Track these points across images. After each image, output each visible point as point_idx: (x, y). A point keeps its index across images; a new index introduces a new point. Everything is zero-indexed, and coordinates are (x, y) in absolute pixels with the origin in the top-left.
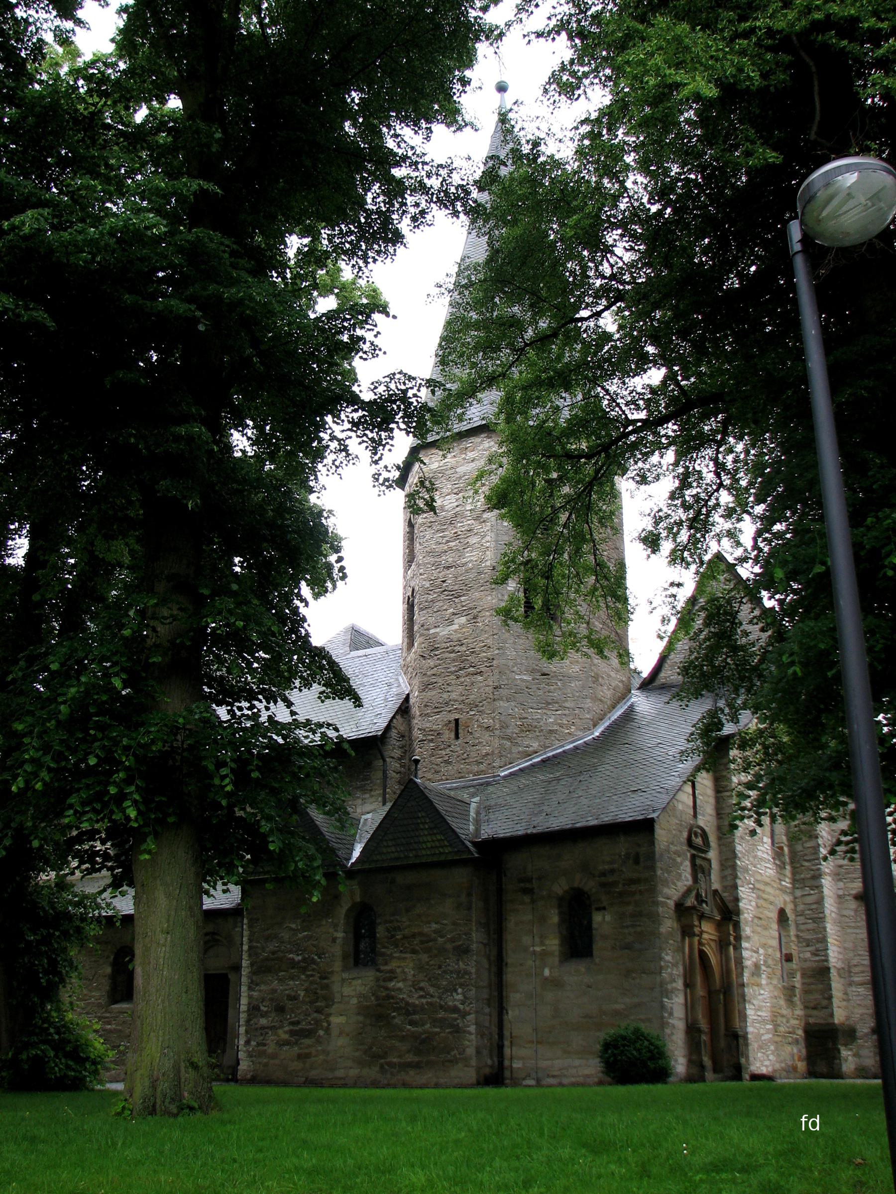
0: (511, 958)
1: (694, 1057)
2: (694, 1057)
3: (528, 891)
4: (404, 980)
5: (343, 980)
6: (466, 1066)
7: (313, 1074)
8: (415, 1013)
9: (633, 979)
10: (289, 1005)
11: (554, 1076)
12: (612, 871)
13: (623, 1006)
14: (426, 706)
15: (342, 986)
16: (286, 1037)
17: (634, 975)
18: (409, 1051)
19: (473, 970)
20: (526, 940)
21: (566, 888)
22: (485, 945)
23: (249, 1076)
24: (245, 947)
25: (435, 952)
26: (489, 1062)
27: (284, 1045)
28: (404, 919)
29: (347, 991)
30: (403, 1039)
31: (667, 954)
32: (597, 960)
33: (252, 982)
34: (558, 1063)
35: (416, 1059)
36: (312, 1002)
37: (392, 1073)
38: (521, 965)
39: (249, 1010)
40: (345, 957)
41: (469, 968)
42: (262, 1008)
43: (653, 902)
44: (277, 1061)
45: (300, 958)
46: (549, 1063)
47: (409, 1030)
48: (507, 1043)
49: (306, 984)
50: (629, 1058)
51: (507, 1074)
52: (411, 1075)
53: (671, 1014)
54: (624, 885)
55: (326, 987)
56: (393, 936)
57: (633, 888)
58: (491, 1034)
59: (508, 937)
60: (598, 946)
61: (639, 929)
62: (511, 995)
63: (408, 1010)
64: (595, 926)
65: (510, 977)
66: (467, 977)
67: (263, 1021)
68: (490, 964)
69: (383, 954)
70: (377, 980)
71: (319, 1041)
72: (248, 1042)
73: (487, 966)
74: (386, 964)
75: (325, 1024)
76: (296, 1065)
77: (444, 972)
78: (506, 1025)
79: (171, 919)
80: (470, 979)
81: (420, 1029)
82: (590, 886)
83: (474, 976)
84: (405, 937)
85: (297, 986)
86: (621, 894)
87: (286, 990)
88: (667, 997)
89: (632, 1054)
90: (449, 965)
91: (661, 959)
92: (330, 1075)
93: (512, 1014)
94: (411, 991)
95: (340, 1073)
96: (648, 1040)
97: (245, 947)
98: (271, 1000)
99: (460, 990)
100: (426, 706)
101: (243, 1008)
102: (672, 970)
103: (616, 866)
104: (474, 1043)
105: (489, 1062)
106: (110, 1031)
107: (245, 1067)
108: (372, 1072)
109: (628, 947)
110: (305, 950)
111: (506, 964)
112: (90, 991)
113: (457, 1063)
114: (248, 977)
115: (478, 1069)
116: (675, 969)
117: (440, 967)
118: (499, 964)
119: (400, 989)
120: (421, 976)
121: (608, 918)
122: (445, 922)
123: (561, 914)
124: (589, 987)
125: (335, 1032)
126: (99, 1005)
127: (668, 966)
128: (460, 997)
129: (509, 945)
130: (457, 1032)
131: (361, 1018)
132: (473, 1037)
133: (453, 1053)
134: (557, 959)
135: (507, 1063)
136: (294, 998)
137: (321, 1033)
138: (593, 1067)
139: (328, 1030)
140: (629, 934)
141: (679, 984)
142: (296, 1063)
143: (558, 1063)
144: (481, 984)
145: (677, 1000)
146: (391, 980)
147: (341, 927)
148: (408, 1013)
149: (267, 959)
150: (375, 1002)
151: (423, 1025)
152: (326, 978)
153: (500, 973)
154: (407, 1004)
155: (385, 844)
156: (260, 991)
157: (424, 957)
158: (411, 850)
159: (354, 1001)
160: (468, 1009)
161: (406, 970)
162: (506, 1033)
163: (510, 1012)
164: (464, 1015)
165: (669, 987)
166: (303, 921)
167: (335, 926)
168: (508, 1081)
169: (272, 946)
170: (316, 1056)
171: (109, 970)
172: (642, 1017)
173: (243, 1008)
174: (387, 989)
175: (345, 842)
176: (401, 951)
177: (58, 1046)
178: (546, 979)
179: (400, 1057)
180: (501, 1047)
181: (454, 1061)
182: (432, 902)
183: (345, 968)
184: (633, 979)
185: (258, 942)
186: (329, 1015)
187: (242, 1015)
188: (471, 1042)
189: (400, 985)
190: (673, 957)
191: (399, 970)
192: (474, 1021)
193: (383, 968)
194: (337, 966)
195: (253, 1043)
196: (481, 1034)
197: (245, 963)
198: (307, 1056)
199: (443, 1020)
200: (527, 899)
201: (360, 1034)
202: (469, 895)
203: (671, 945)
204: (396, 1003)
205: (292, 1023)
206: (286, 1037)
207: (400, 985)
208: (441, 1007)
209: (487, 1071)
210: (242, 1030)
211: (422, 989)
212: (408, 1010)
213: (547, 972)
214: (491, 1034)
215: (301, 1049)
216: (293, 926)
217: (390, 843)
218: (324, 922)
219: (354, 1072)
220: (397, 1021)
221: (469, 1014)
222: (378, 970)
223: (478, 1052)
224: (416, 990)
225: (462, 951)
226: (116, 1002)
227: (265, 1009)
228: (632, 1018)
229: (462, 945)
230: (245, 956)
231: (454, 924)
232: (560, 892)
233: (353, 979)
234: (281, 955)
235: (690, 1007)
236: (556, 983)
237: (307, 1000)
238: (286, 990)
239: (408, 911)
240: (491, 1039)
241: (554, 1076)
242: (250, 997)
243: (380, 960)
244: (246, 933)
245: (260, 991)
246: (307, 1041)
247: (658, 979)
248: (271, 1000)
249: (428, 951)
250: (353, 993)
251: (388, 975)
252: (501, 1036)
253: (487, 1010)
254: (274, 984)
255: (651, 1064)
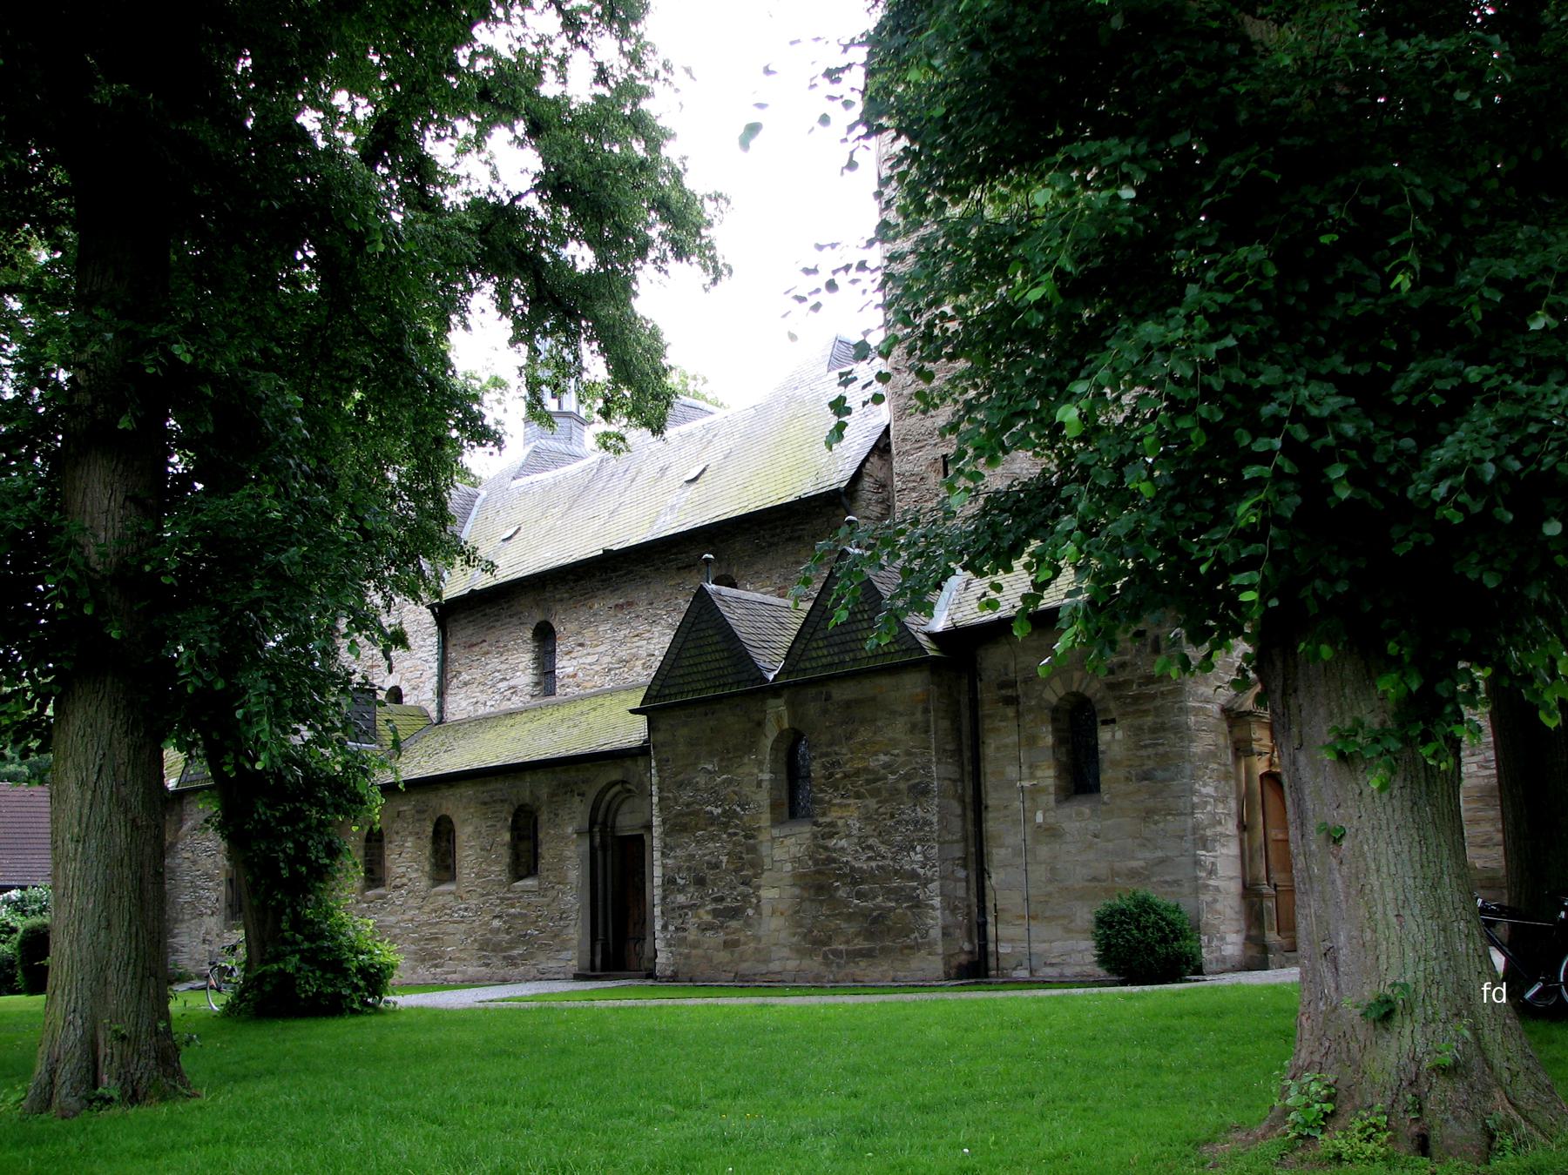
0: (992, 799)
1: (1254, 932)
2: (1254, 932)
3: (1012, 701)
4: (848, 836)
5: (773, 839)
6: (930, 954)
7: (745, 967)
8: (863, 882)
9: (1156, 823)
10: (710, 875)
11: (1052, 965)
12: (1123, 665)
13: (1142, 863)
14: (904, 440)
15: (772, 848)
16: (708, 918)
17: (1156, 818)
18: (857, 935)
19: (935, 819)
20: (1012, 771)
21: (1062, 693)
22: (954, 781)
23: (668, 973)
24: (655, 799)
25: (885, 794)
26: (967, 947)
27: (706, 929)
28: (844, 751)
29: (778, 853)
30: (850, 918)
31: (1205, 785)
32: (1106, 798)
33: (666, 846)
34: (1058, 946)
35: (866, 945)
36: (737, 871)
37: (838, 965)
38: (1006, 807)
39: (663, 884)
40: (774, 806)
41: (929, 816)
42: (679, 881)
43: (1181, 709)
44: (700, 952)
45: (720, 810)
46: (1046, 946)
47: (856, 905)
48: (990, 919)
49: (730, 846)
50: (1128, 941)
51: (992, 962)
52: (861, 968)
53: (1212, 872)
54: (1140, 685)
55: (753, 849)
56: (831, 775)
57: (1152, 689)
58: (969, 906)
59: (988, 768)
60: (1107, 776)
61: (1161, 750)
62: (994, 851)
63: (853, 877)
64: (1101, 747)
65: (992, 825)
66: (927, 829)
67: (681, 899)
68: (964, 809)
69: (821, 801)
70: (815, 836)
71: (748, 925)
72: (665, 927)
73: (959, 811)
74: (824, 814)
75: (754, 900)
76: (723, 956)
77: (898, 822)
78: (990, 894)
79: (85, 819)
80: (932, 832)
81: (870, 904)
82: (1094, 689)
83: (936, 827)
84: (846, 776)
85: (717, 849)
86: (1136, 699)
87: (705, 855)
88: (1205, 848)
89: (1132, 935)
90: (903, 813)
91: (1193, 792)
92: (763, 968)
93: (996, 878)
94: (857, 851)
95: (775, 966)
96: (1155, 912)
97: (655, 799)
98: (689, 869)
99: (919, 848)
100: (904, 440)
101: (657, 881)
102: (1215, 806)
103: (1128, 658)
104: (940, 922)
105: (967, 947)
106: (514, 916)
107: (664, 961)
108: (814, 964)
109: (1146, 776)
110: (725, 799)
111: (986, 807)
112: (489, 865)
113: (919, 950)
114: (662, 840)
115: (947, 958)
116: (1221, 805)
117: (892, 816)
118: (977, 808)
119: (843, 849)
120: (869, 830)
121: (1119, 735)
122: (896, 752)
123: (1056, 731)
124: (1096, 836)
125: (766, 910)
126: (500, 883)
127: (1206, 803)
128: (919, 857)
129: (990, 781)
130: (918, 906)
131: (797, 891)
132: (938, 913)
133: (913, 936)
134: (1052, 798)
135: (991, 947)
136: (716, 866)
137: (750, 912)
138: (1083, 952)
139: (757, 907)
140: (1149, 757)
141: (1231, 827)
142: (722, 954)
143: (1058, 946)
144: (949, 838)
145: (1224, 851)
146: (831, 836)
147: (767, 767)
148: (854, 883)
149: (680, 814)
150: (813, 868)
151: (874, 898)
152: (753, 837)
153: (979, 822)
154: (853, 869)
155: (815, 645)
156: (675, 857)
157: (872, 803)
158: (847, 652)
159: (788, 866)
160: (929, 874)
161: (850, 822)
162: (990, 905)
163: (993, 875)
164: (926, 882)
165: (1209, 832)
166: (721, 760)
167: (760, 763)
168: (993, 973)
169: (686, 796)
170: (745, 944)
171: (507, 837)
172: (1168, 878)
173: (657, 881)
174: (826, 848)
175: (773, 645)
176: (842, 796)
177: (310, 958)
178: (1039, 826)
179: (847, 942)
180: (983, 926)
181: (916, 947)
182: (879, 724)
183: (776, 822)
184: (1156, 823)
185: (669, 791)
186: (759, 887)
187: (656, 892)
188: (936, 919)
189: (843, 843)
190: (1216, 788)
191: (840, 823)
192: (938, 891)
193: (821, 820)
194: (765, 819)
195: (671, 928)
196: (950, 906)
197: (656, 821)
198: (736, 944)
199: (896, 891)
200: (1011, 712)
201: (798, 912)
202: (926, 711)
203: (1213, 770)
204: (840, 869)
205: (716, 900)
206: (708, 918)
207: (843, 843)
208: (896, 872)
209: (963, 958)
210: (657, 911)
211: (870, 847)
212: (854, 878)
213: (1039, 818)
214: (969, 906)
215: (727, 934)
216: (710, 767)
217: (821, 644)
218: (746, 760)
219: (792, 964)
220: (841, 893)
221: (933, 881)
222: (816, 824)
223: (946, 933)
224: (863, 849)
225: (920, 792)
226: (520, 878)
227: (681, 882)
228: (1155, 880)
229: (918, 784)
230: (655, 811)
231: (908, 753)
232: (1054, 700)
233: (785, 837)
234: (698, 807)
235: (1245, 858)
236: (1052, 833)
237: (732, 867)
238: (705, 855)
239: (848, 739)
240: (968, 914)
241: (1052, 965)
242: (664, 866)
243: (817, 809)
244: (655, 780)
245: (675, 857)
246: (734, 924)
247: (1190, 822)
248: (689, 869)
249: (875, 793)
250: (786, 857)
251: (827, 830)
252: (982, 910)
253: (961, 874)
254: (693, 849)
255: (1161, 950)
